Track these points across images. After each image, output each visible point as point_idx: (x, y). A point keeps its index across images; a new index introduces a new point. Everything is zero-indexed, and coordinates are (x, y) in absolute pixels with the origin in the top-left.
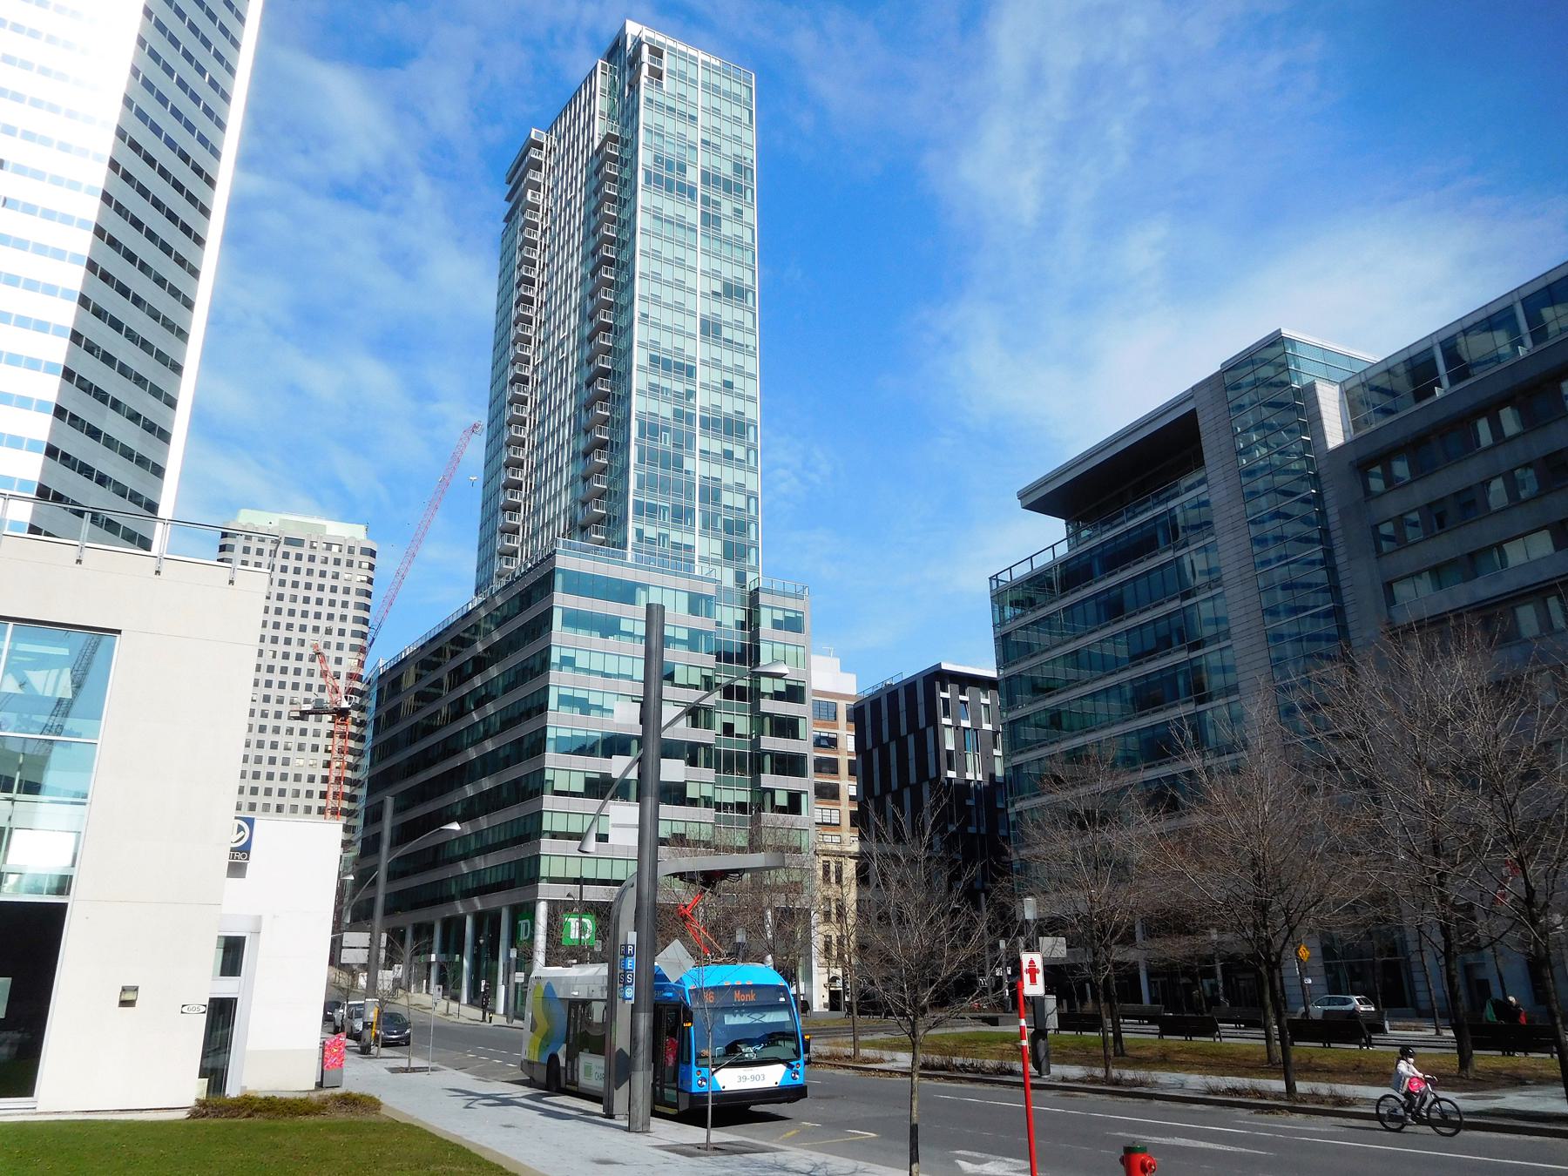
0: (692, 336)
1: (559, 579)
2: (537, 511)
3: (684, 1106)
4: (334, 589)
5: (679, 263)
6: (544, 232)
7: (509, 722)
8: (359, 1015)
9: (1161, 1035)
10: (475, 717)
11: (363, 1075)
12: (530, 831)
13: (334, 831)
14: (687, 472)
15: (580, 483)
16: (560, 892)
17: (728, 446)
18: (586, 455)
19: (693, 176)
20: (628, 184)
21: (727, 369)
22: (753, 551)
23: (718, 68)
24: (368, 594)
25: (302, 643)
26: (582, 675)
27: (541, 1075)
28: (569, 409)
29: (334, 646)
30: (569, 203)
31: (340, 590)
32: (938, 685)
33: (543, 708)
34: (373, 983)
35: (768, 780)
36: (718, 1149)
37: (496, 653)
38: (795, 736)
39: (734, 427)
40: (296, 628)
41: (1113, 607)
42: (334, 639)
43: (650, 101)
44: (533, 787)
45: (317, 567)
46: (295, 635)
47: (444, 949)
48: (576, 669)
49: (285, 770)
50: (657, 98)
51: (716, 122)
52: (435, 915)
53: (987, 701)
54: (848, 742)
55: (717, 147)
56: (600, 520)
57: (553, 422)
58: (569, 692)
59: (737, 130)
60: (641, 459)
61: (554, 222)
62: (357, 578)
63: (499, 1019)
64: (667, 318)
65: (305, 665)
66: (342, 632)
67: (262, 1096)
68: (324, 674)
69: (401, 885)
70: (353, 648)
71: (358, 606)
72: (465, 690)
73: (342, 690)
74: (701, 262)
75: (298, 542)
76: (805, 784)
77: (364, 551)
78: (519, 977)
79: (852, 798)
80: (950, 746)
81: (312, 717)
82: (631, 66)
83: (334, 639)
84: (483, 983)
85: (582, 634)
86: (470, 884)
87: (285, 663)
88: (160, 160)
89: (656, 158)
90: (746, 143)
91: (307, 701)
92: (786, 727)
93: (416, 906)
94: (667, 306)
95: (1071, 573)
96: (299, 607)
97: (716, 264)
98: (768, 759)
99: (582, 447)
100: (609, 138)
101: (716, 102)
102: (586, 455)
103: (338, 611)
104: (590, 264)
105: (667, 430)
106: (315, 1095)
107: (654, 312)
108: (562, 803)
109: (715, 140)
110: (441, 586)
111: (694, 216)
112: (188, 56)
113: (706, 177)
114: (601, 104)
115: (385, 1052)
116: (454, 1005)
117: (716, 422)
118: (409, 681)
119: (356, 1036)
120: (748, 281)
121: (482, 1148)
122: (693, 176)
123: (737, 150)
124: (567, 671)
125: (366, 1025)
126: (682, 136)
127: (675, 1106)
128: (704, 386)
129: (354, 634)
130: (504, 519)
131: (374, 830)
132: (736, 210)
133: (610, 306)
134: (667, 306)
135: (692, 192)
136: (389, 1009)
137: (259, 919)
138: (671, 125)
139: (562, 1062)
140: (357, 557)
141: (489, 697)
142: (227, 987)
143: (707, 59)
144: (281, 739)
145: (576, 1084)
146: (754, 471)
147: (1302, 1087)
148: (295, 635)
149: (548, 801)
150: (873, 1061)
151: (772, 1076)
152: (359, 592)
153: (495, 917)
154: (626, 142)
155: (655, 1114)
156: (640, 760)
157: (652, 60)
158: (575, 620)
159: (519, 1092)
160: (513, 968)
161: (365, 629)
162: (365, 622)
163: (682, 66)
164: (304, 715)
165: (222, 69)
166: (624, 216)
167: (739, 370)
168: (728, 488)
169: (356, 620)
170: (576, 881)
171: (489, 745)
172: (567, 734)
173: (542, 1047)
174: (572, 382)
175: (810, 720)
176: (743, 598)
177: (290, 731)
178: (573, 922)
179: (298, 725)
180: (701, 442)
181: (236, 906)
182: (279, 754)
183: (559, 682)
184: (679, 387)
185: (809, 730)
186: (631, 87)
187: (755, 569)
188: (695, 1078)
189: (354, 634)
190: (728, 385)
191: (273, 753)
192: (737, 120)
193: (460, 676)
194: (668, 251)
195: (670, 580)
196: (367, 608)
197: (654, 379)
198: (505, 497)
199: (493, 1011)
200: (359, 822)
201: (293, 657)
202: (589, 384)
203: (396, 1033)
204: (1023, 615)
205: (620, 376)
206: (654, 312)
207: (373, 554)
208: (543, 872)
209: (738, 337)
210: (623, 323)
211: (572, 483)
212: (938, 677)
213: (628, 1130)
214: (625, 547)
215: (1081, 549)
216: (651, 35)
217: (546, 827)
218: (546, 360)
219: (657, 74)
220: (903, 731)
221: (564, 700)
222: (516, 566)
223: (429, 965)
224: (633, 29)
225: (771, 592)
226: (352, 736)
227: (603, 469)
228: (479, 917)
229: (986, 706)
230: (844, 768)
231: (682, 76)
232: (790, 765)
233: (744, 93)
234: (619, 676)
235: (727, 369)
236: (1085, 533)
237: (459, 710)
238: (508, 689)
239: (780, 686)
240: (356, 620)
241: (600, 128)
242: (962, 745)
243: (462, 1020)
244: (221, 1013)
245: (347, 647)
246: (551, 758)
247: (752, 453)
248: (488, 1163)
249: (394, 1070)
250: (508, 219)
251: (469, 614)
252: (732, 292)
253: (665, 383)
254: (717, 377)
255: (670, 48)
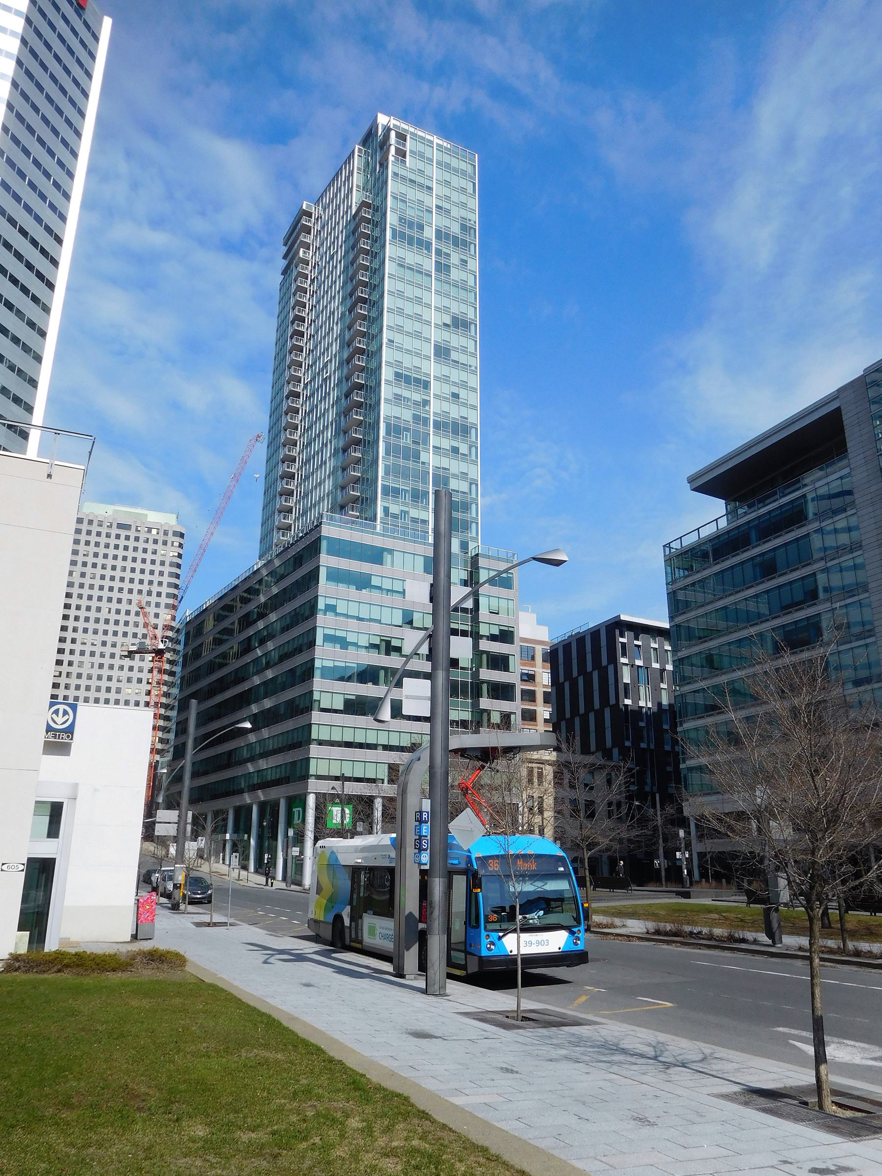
0: (428, 358)
1: (324, 545)
2: (306, 495)
3: (473, 968)
4: (153, 562)
5: (419, 301)
6: (312, 281)
7: (284, 657)
8: (171, 878)
9: (749, 903)
10: (259, 652)
11: (173, 931)
12: (302, 739)
13: (146, 717)
14: (423, 463)
15: (340, 472)
16: (325, 787)
17: (455, 444)
18: (345, 450)
19: (430, 233)
20: (379, 241)
21: (455, 384)
22: (474, 525)
23: (446, 148)
24: (179, 566)
25: (130, 602)
26: (341, 618)
27: (327, 933)
28: (331, 415)
29: (153, 605)
30: (332, 257)
31: (158, 563)
32: (617, 632)
33: (312, 644)
34: (181, 852)
35: (485, 703)
36: (526, 1019)
37: (275, 603)
38: (506, 668)
39: (460, 429)
40: (126, 591)
41: (767, 568)
42: (154, 599)
43: (396, 174)
44: (304, 706)
45: (141, 545)
46: (125, 596)
47: (236, 830)
48: (337, 614)
49: (118, 696)
50: (401, 172)
51: (447, 192)
52: (229, 804)
53: (656, 646)
54: (544, 678)
55: (448, 211)
56: (356, 500)
57: (319, 426)
58: (332, 632)
59: (463, 198)
60: (387, 453)
61: (320, 273)
62: (170, 553)
63: (279, 884)
64: (408, 343)
65: (132, 618)
66: (159, 594)
67: (73, 951)
68: (146, 625)
69: (203, 781)
70: (167, 606)
71: (171, 575)
72: (251, 631)
73: (159, 636)
74: (434, 300)
75: (127, 527)
76: (515, 706)
77: (175, 534)
78: (295, 851)
79: (546, 721)
80: (627, 679)
81: (137, 656)
82: (381, 148)
83: (154, 599)
84: (266, 856)
85: (342, 587)
86: (256, 781)
87: (117, 617)
88: (20, 222)
89: (400, 219)
90: (471, 209)
91: (133, 644)
92: (500, 662)
93: (215, 797)
94: (408, 334)
95: (721, 546)
96: (128, 575)
97: (446, 302)
98: (485, 687)
99: (341, 444)
100: (364, 204)
101: (447, 176)
102: (345, 450)
103: (156, 578)
104: (349, 303)
105: (408, 430)
106: (124, 949)
107: (398, 338)
108: (326, 717)
109: (446, 205)
110: (235, 555)
111: (430, 264)
112: (41, 141)
113: (439, 234)
114: (357, 179)
115: (191, 908)
116: (244, 873)
117: (445, 425)
118: (210, 624)
119: (169, 896)
120: (471, 315)
121: (293, 1019)
122: (430, 233)
123: (464, 213)
124: (330, 616)
125: (176, 886)
126: (421, 202)
127: (463, 967)
128: (436, 396)
129: (168, 595)
130: (281, 502)
131: (181, 739)
132: (462, 260)
133: (364, 335)
134: (408, 334)
135: (428, 246)
136: (193, 874)
137: (75, 786)
138: (413, 194)
139: (347, 922)
140: (170, 538)
141: (271, 636)
142: (45, 849)
143: (441, 142)
144: (115, 673)
145: (361, 942)
146: (475, 462)
147: (851, 945)
148: (125, 596)
149: (316, 716)
150: (606, 926)
151: (555, 942)
152: (172, 564)
153: (275, 805)
154: (380, 210)
155: (450, 976)
156: (430, 636)
157: (397, 143)
158: (336, 576)
159: (309, 948)
160: (290, 844)
161: (176, 592)
162: (176, 586)
163: (420, 147)
164: (130, 655)
165: (68, 153)
166: (375, 265)
167: (464, 385)
168: (455, 476)
169: (170, 585)
170: (337, 778)
171: (270, 674)
172: (330, 664)
173: (327, 909)
174: (334, 395)
175: (518, 657)
176: (466, 562)
177: (121, 668)
178: (336, 810)
179: (127, 662)
180: (433, 440)
181: (54, 776)
182: (114, 685)
183: (324, 623)
184: (417, 397)
185: (517, 666)
186: (381, 165)
187: (475, 539)
188: (484, 942)
189: (168, 595)
190: (456, 396)
191: (109, 684)
192: (463, 190)
193: (247, 621)
194: (409, 291)
195: (409, 547)
196: (178, 576)
197: (398, 391)
198: (281, 485)
199: (274, 878)
200: (171, 736)
201: (123, 612)
202: (347, 396)
203: (200, 893)
204: (688, 576)
205: (372, 389)
206: (398, 338)
207: (182, 535)
208: (312, 771)
209: (463, 358)
210: (373, 348)
211: (333, 472)
212: (617, 626)
213: (425, 992)
214: (375, 520)
215: (741, 521)
216: (398, 123)
217: (314, 736)
218: (313, 379)
219: (401, 154)
220: (589, 668)
221: (328, 638)
222: (288, 538)
223: (225, 841)
224: (383, 120)
225: (488, 557)
226: (165, 672)
227: (358, 461)
228: (262, 806)
229: (655, 649)
230: (540, 698)
231: (421, 156)
232: (502, 691)
233: (469, 169)
234: (370, 620)
235: (455, 384)
236: (740, 511)
237: (247, 647)
238: (285, 629)
239: (495, 631)
240: (170, 585)
241: (356, 198)
242: (636, 679)
243: (250, 884)
244: (40, 874)
245: (163, 605)
246: (318, 683)
247: (473, 449)
248: (305, 1043)
249: (198, 925)
250: (284, 272)
251: (255, 573)
252: (459, 324)
253: (406, 394)
254: (447, 389)
255: (412, 133)
